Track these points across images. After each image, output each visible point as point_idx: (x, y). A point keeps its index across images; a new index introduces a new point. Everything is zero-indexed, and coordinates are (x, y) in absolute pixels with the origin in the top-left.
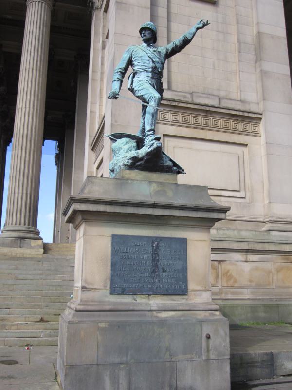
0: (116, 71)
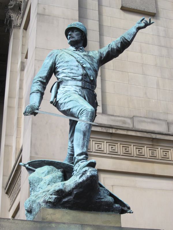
0: (34, 81)
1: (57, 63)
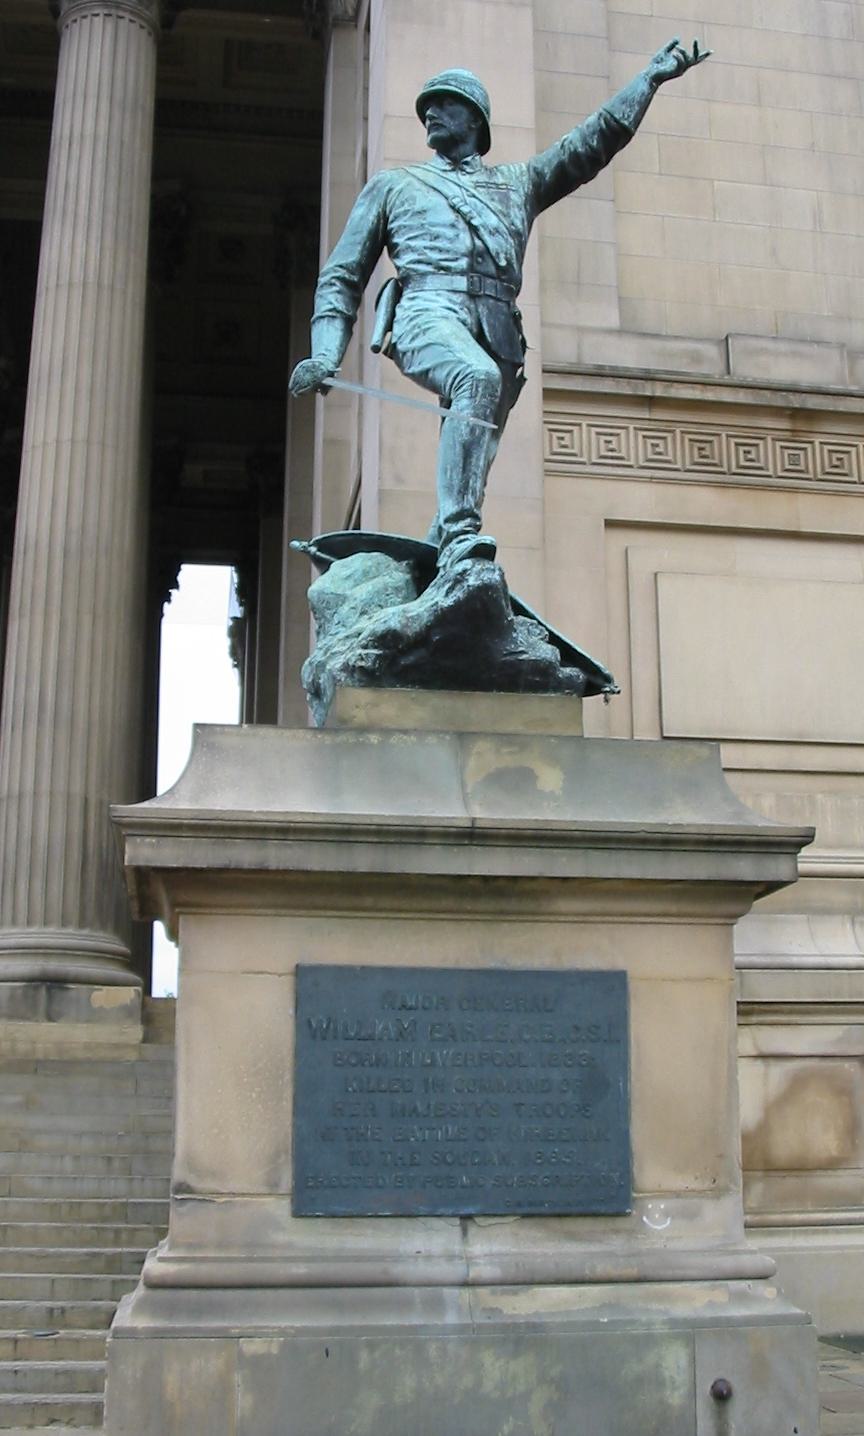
1: (391, 218)
